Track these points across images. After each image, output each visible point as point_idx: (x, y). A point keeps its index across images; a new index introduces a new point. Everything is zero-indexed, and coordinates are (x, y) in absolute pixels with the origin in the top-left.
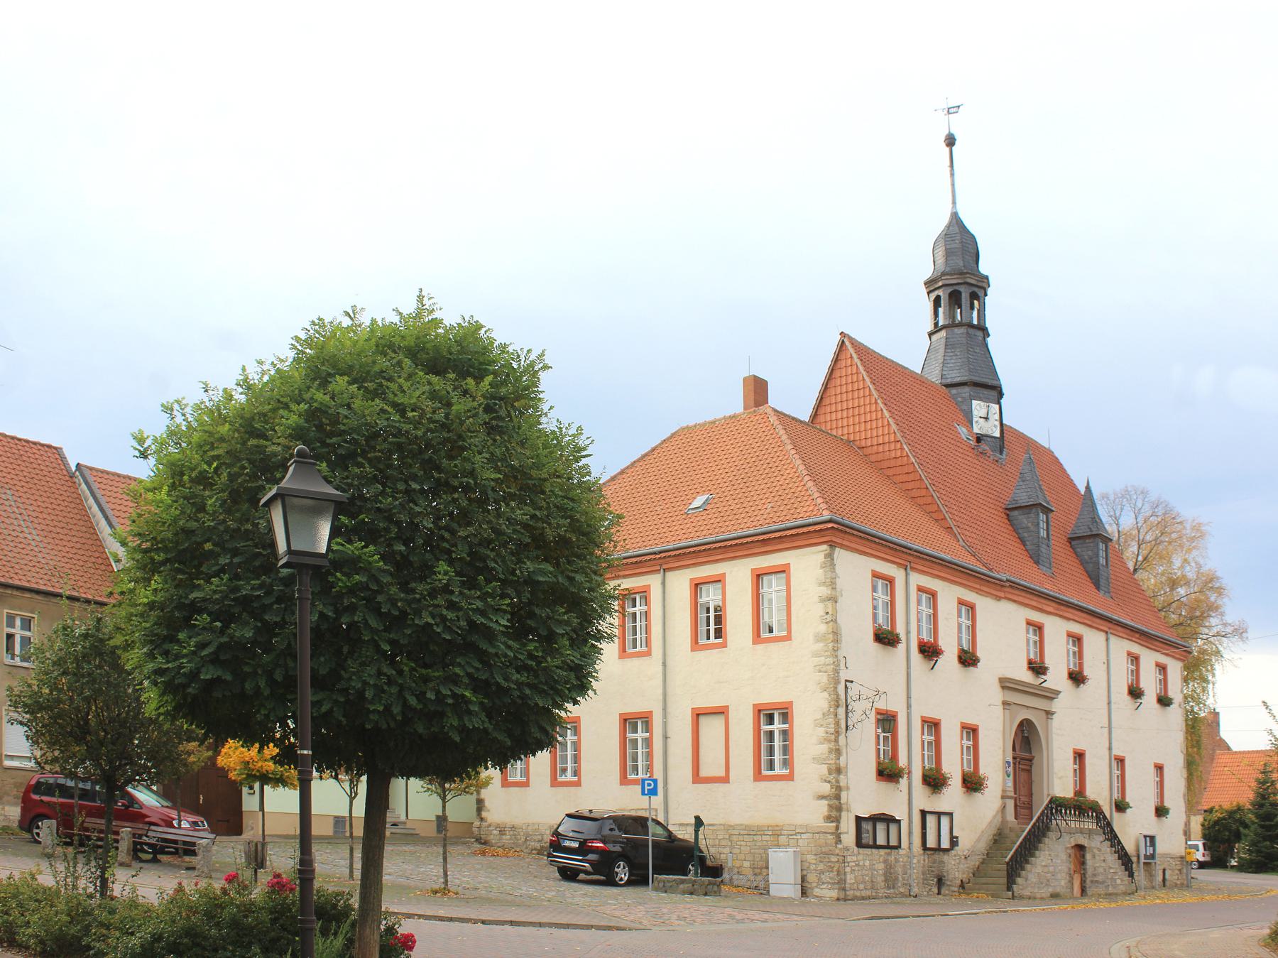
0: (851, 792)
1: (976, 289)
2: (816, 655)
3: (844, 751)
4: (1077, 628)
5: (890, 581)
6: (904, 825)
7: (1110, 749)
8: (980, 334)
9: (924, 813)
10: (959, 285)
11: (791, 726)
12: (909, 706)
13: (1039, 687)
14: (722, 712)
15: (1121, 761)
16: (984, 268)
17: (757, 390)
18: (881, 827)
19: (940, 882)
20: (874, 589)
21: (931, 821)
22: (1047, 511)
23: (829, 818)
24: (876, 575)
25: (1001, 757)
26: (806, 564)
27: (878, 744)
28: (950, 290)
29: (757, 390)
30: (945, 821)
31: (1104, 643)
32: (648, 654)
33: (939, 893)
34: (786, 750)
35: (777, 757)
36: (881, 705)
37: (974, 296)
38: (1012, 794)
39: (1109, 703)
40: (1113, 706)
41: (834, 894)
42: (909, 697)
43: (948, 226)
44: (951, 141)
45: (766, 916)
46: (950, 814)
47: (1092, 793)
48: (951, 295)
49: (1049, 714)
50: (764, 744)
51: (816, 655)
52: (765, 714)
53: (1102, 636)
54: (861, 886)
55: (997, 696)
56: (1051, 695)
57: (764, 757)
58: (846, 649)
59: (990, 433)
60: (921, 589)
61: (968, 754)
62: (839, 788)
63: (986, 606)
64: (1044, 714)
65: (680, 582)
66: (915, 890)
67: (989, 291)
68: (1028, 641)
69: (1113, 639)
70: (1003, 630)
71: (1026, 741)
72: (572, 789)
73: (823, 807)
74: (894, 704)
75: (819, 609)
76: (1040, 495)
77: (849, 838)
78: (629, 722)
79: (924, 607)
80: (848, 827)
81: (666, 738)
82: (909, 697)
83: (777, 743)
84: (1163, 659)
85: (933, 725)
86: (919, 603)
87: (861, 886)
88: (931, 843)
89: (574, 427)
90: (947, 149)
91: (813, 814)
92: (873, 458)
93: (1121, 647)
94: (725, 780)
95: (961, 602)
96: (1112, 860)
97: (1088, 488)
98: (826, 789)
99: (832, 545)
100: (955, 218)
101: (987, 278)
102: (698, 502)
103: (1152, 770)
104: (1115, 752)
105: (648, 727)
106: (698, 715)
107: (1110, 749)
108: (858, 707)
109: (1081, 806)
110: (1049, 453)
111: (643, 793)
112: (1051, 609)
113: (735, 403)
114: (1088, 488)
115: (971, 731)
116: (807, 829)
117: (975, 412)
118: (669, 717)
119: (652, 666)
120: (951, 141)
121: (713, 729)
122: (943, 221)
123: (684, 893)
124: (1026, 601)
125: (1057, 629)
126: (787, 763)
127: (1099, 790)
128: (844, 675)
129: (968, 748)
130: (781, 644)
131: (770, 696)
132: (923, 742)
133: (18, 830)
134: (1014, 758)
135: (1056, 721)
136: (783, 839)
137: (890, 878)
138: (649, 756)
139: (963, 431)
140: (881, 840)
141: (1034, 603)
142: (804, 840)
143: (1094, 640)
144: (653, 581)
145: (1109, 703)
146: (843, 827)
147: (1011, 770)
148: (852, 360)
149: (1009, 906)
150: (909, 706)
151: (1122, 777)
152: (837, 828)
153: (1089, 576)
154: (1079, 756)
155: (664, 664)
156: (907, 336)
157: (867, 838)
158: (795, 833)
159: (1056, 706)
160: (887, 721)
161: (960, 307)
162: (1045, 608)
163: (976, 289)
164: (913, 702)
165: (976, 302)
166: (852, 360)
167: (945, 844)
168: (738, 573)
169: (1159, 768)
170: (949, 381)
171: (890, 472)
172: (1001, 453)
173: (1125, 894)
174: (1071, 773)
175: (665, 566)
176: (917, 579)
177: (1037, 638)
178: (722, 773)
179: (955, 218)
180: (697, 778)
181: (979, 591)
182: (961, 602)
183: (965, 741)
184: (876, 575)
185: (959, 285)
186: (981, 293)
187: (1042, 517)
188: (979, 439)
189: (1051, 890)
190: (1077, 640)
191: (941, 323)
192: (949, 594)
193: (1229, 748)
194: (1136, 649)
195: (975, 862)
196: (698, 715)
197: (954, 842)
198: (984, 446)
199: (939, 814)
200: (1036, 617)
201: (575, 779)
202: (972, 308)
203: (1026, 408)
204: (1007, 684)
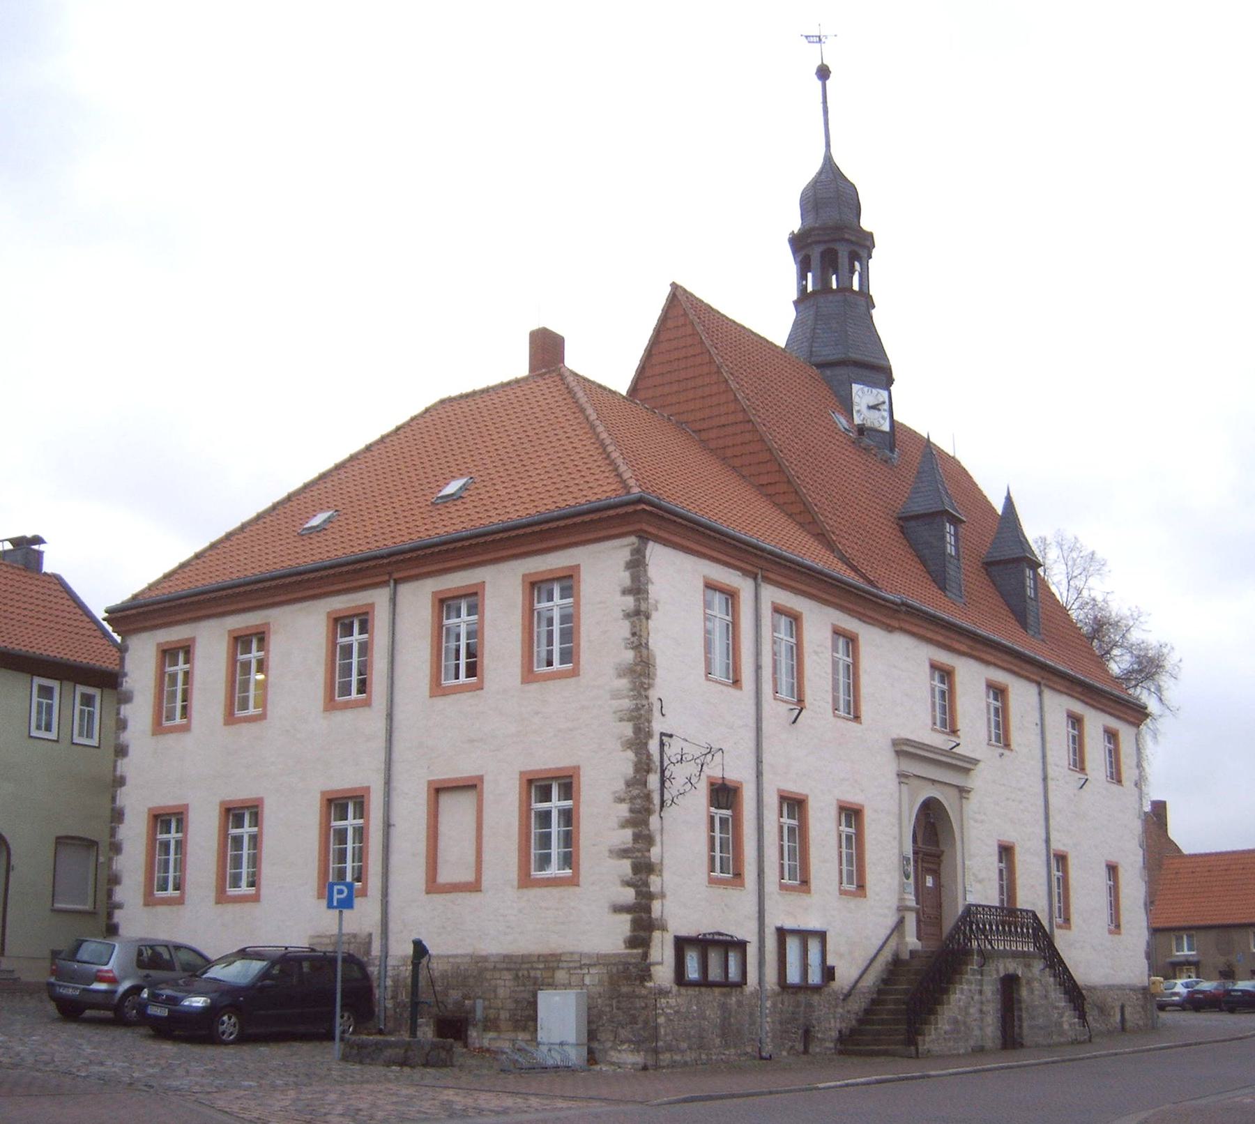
0: (667, 902)
1: (856, 248)
2: (616, 695)
3: (658, 838)
4: (1000, 677)
5: (731, 595)
6: (752, 951)
7: (1048, 841)
8: (862, 301)
9: (782, 933)
10: (832, 236)
11: (577, 804)
12: (759, 774)
13: (949, 753)
14: (471, 786)
15: (1062, 859)
16: (866, 223)
17: (547, 348)
18: (714, 958)
19: (807, 1035)
20: (707, 605)
21: (793, 945)
22: (955, 521)
23: (632, 942)
24: (710, 586)
25: (896, 851)
26: (601, 568)
27: (712, 829)
28: (821, 248)
29: (547, 348)
30: (814, 947)
31: (1035, 698)
32: (367, 703)
33: (806, 1051)
34: (569, 839)
35: (555, 850)
36: (714, 770)
37: (854, 256)
38: (913, 904)
39: (1045, 779)
40: (1051, 784)
41: (638, 1059)
42: (759, 761)
43: (820, 173)
44: (823, 73)
45: (509, 1102)
46: (822, 936)
47: (1025, 900)
48: (823, 254)
49: (963, 791)
50: (535, 831)
51: (616, 695)
52: (538, 785)
53: (1032, 690)
54: (684, 1045)
55: (888, 766)
56: (965, 766)
57: (534, 852)
58: (664, 685)
59: (876, 425)
60: (778, 610)
61: (849, 846)
62: (650, 896)
63: (872, 639)
64: (955, 792)
65: (417, 599)
66: (768, 1049)
67: (875, 253)
68: (933, 690)
69: (1048, 694)
70: (897, 670)
71: (932, 832)
72: (248, 907)
73: (623, 925)
74: (738, 771)
75: (624, 629)
76: (946, 500)
77: (663, 974)
78: (337, 804)
79: (783, 635)
80: (662, 952)
81: (388, 825)
82: (759, 761)
83: (555, 829)
84: (1113, 723)
85: (794, 805)
86: (775, 628)
87: (684, 1045)
88: (793, 976)
89: (615, 703)
90: (819, 83)
91: (607, 936)
92: (712, 445)
93: (1059, 705)
94: (474, 887)
95: (837, 632)
96: (1058, 997)
97: (1009, 502)
98: (628, 895)
99: (644, 537)
100: (829, 162)
101: (871, 235)
102: (452, 488)
103: (1103, 872)
104: (1056, 846)
105: (361, 811)
106: (439, 790)
107: (1048, 841)
108: (679, 774)
109: (1010, 916)
110: (952, 462)
111: (330, 906)
112: (964, 648)
113: (518, 365)
114: (1009, 502)
115: (851, 814)
116: (601, 960)
117: (856, 399)
118: (394, 795)
119: (371, 721)
120: (823, 73)
121: (457, 811)
122: (814, 166)
123: (388, 1063)
124: (930, 634)
125: (972, 677)
126: (569, 860)
127: (1032, 895)
128: (658, 726)
129: (849, 838)
130: (564, 682)
131: (547, 759)
132: (781, 828)
133: (675, 989)
134: (915, 853)
135: (973, 804)
136: (561, 975)
137: (728, 1032)
138: (361, 855)
139: (842, 421)
140: (714, 973)
141: (940, 639)
142: (592, 978)
143: (1022, 694)
144: (379, 598)
145: (1045, 779)
146: (655, 955)
147: (911, 869)
148: (685, 327)
149: (912, 1068)
150: (759, 774)
151: (1064, 882)
152: (645, 955)
153: (1013, 612)
154: (1006, 852)
155: (390, 716)
156: (764, 300)
157: (693, 972)
158: (582, 963)
159: (978, 781)
160: (724, 794)
161: (836, 272)
162: (957, 646)
163: (856, 248)
164: (766, 768)
165: (857, 265)
166: (685, 327)
167: (815, 977)
168: (503, 585)
169: (1112, 869)
170: (820, 360)
171: (737, 462)
172: (892, 451)
173: (1075, 1042)
174: (996, 876)
175: (396, 575)
176: (772, 595)
177: (945, 687)
178: (468, 876)
179: (829, 162)
180: (433, 886)
181: (862, 617)
182: (837, 632)
183: (843, 828)
184: (710, 586)
185: (832, 236)
186: (864, 254)
187: (949, 528)
188: (861, 430)
189: (972, 1043)
190: (998, 692)
191: (810, 289)
192: (819, 621)
193: (1178, 850)
194: (1078, 707)
195: (857, 1005)
196: (439, 790)
197: (829, 973)
198: (866, 441)
199: (804, 935)
200: (944, 658)
201: (252, 890)
202: (852, 271)
203: (929, 397)
204: (904, 749)
